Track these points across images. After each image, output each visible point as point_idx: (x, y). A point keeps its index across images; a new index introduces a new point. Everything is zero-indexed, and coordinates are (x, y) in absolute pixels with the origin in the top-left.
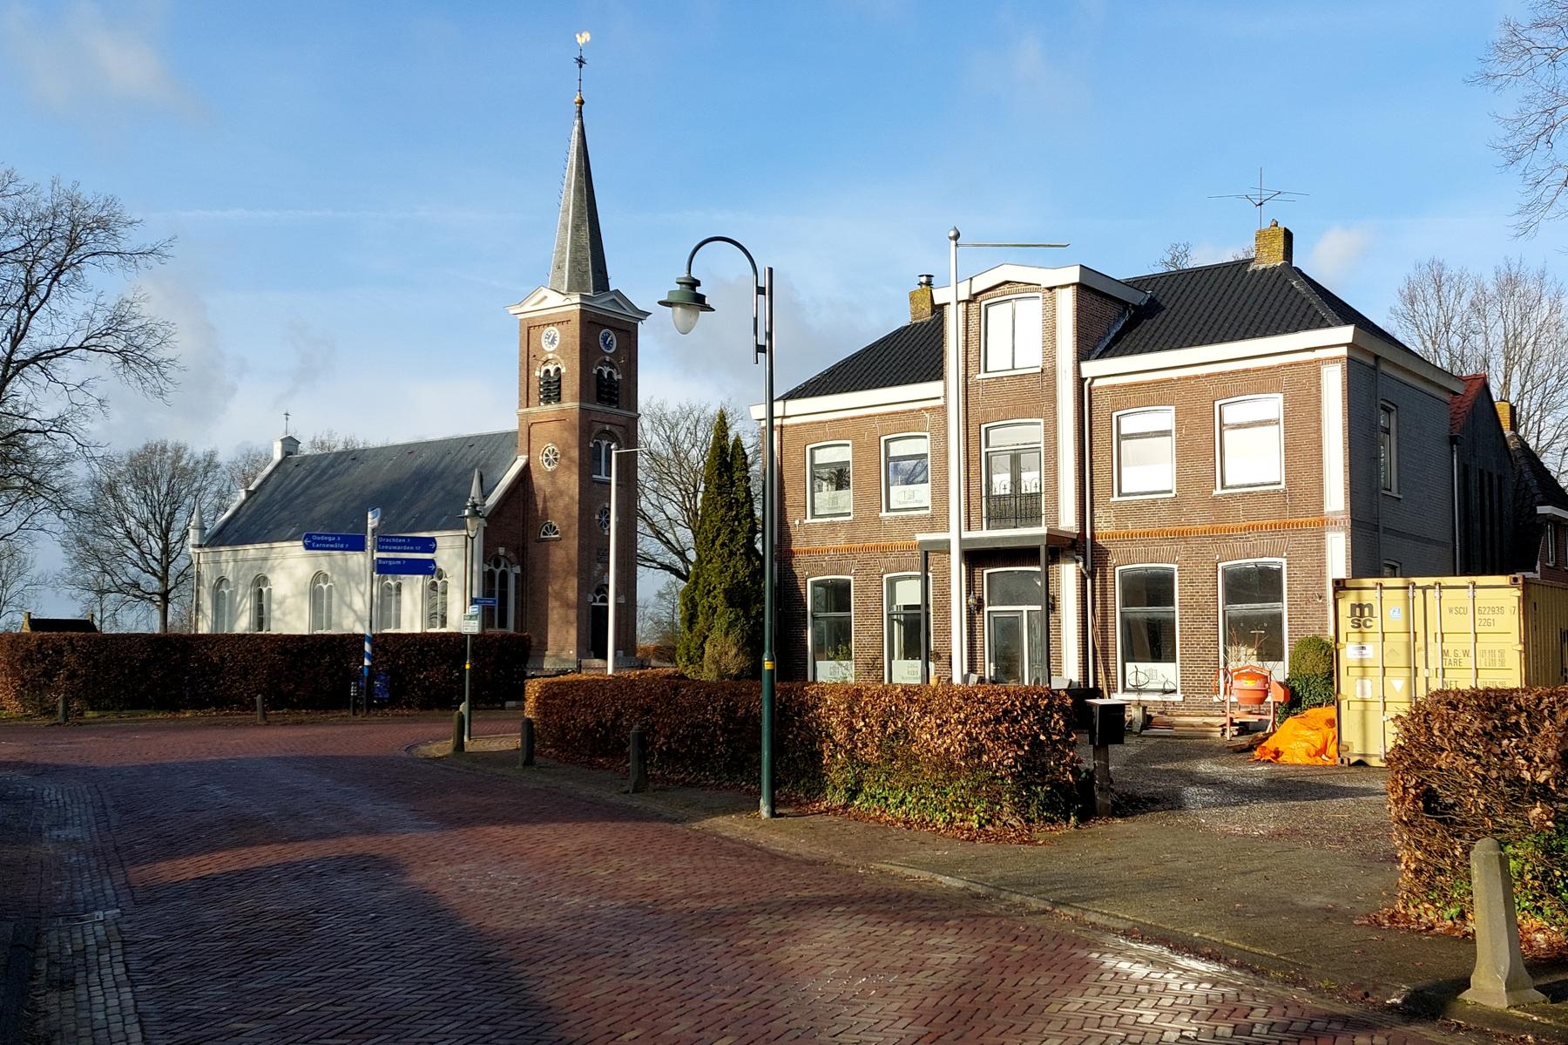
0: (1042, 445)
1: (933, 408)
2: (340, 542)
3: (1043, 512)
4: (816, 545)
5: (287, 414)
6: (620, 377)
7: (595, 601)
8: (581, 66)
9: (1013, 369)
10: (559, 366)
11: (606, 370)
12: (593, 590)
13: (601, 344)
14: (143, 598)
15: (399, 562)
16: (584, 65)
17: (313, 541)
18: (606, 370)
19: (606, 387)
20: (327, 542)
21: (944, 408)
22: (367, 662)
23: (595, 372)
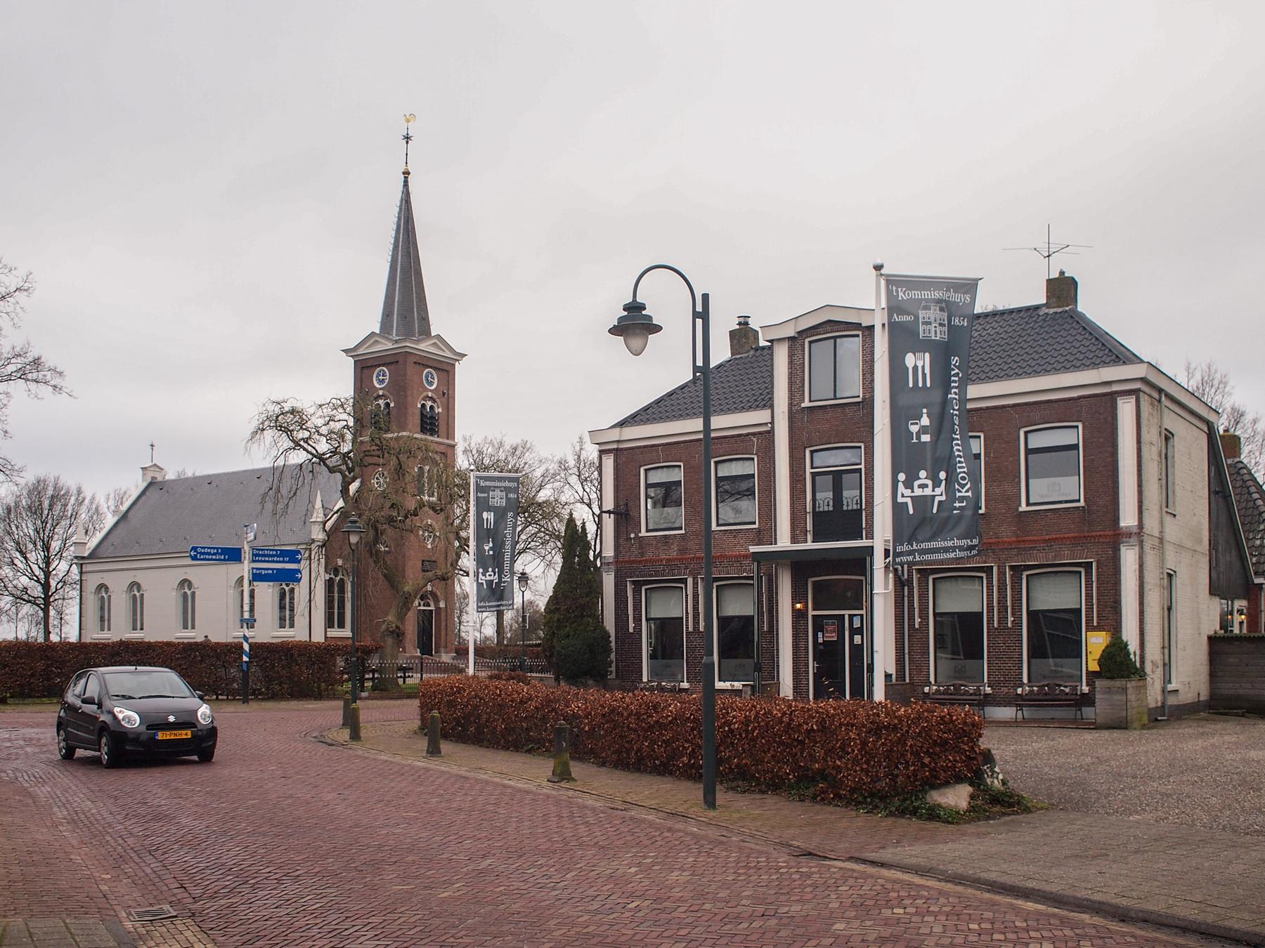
0: (862, 466)
1: (760, 433)
2: (221, 554)
3: (864, 526)
4: (649, 555)
5: (152, 446)
6: (440, 410)
7: (420, 605)
8: (407, 142)
9: (835, 398)
10: (388, 401)
11: (429, 403)
12: (418, 597)
13: (425, 382)
14: (29, 601)
15: (270, 572)
16: (410, 142)
17: (198, 553)
18: (429, 403)
19: (428, 419)
20: (209, 554)
21: (771, 433)
22: (245, 659)
23: (419, 406)
